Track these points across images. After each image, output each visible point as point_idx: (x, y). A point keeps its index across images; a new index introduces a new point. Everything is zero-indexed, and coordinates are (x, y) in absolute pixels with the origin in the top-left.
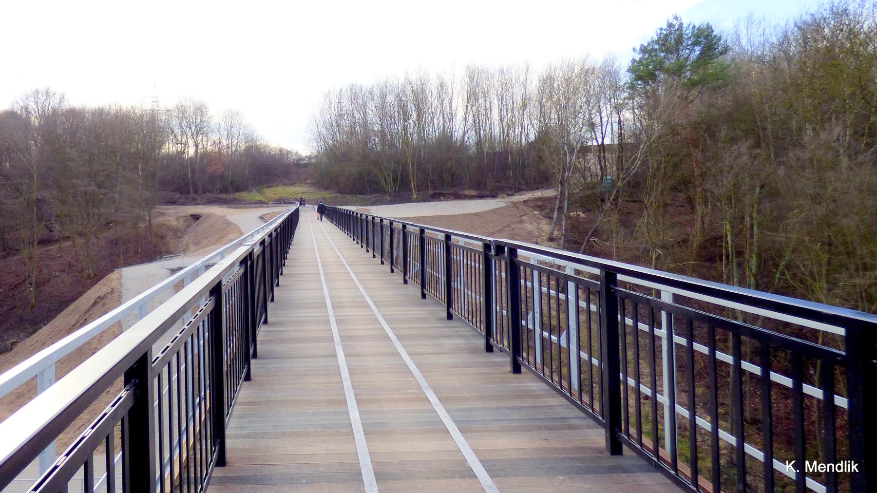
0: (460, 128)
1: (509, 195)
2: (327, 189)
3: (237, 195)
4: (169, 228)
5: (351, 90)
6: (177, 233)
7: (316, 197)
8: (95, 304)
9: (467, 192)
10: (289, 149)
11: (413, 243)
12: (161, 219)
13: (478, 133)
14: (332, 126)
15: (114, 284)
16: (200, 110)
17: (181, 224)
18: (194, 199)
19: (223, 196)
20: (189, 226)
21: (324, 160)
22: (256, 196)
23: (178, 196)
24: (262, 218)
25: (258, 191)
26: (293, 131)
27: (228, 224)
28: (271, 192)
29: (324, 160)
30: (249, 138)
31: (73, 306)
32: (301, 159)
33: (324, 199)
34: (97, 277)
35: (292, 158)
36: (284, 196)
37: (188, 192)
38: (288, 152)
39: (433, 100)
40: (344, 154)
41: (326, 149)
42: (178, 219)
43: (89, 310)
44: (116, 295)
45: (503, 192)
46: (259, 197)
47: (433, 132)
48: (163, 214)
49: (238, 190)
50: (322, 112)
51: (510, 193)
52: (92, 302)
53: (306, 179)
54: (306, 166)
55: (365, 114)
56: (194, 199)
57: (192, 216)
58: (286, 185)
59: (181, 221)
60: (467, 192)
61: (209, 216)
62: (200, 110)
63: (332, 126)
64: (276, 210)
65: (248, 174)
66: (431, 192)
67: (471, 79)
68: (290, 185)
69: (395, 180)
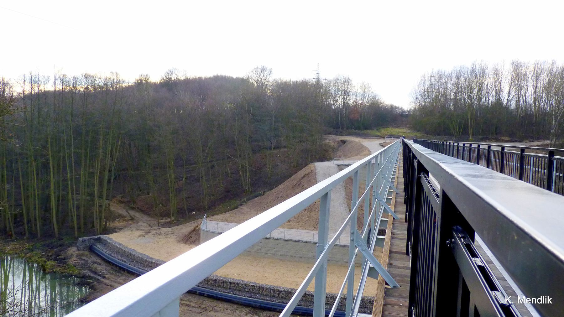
0: (507, 95)
1: (530, 141)
3: (366, 131)
4: (330, 147)
5: (438, 74)
6: (334, 150)
7: (411, 135)
8: (304, 177)
9: (504, 138)
13: (518, 101)
14: (424, 94)
15: (312, 169)
16: (347, 82)
17: (336, 145)
18: (341, 132)
19: (358, 132)
20: (339, 146)
23: (332, 130)
24: (381, 144)
26: (402, 95)
27: (363, 146)
28: (385, 131)
29: (418, 113)
32: (403, 112)
33: (416, 137)
35: (399, 111)
36: (393, 133)
37: (338, 128)
38: (396, 107)
41: (420, 108)
45: (527, 139)
46: (378, 133)
49: (366, 129)
51: (532, 140)
54: (407, 116)
55: (446, 88)
56: (341, 132)
58: (393, 127)
59: (336, 144)
60: (504, 138)
61: (351, 142)
62: (347, 82)
63: (424, 94)
64: (389, 141)
65: (375, 119)
66: (480, 137)
67: (516, 70)
68: (396, 127)
69: (459, 129)
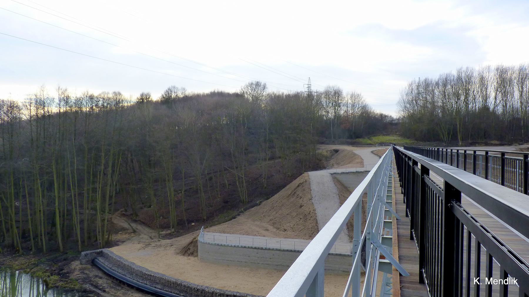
2: (408, 138)
3: (357, 140)
4: (323, 156)
6: (328, 159)
8: (298, 186)
9: (493, 142)
10: (386, 114)
11: (440, 158)
12: (320, 151)
15: (306, 178)
17: (328, 154)
20: (332, 155)
21: (407, 121)
22: (367, 141)
25: (369, 138)
26: (388, 101)
27: (355, 155)
28: (376, 139)
30: (364, 107)
31: (288, 187)
32: (393, 120)
33: (407, 143)
34: (294, 177)
35: (388, 120)
38: (386, 116)
39: (475, 87)
40: (419, 119)
41: (409, 116)
42: (327, 152)
43: (296, 188)
44: (308, 183)
46: (369, 142)
47: (477, 105)
48: (319, 149)
49: (358, 137)
50: (407, 95)
52: (297, 185)
53: (396, 132)
54: (396, 124)
57: (334, 150)
58: (384, 135)
59: (329, 153)
60: (493, 142)
61: (343, 151)
66: (470, 141)
68: (387, 135)
69: (449, 134)
